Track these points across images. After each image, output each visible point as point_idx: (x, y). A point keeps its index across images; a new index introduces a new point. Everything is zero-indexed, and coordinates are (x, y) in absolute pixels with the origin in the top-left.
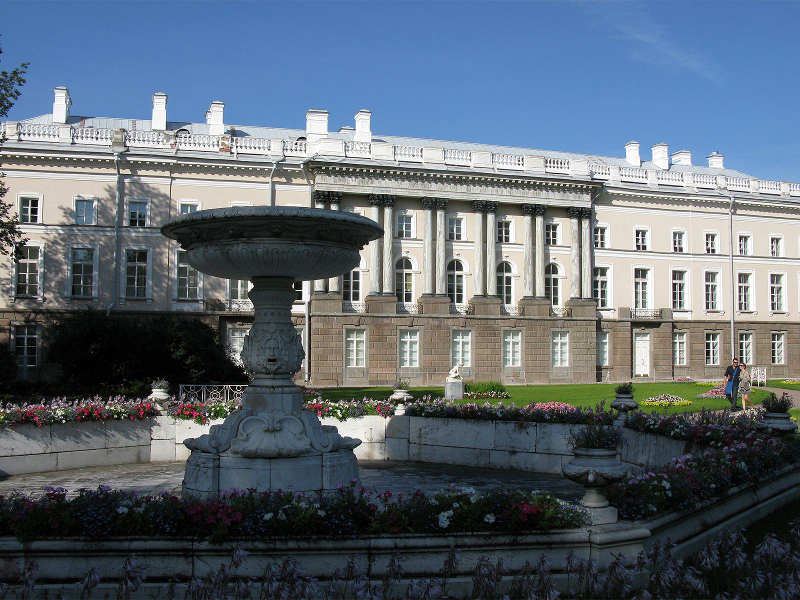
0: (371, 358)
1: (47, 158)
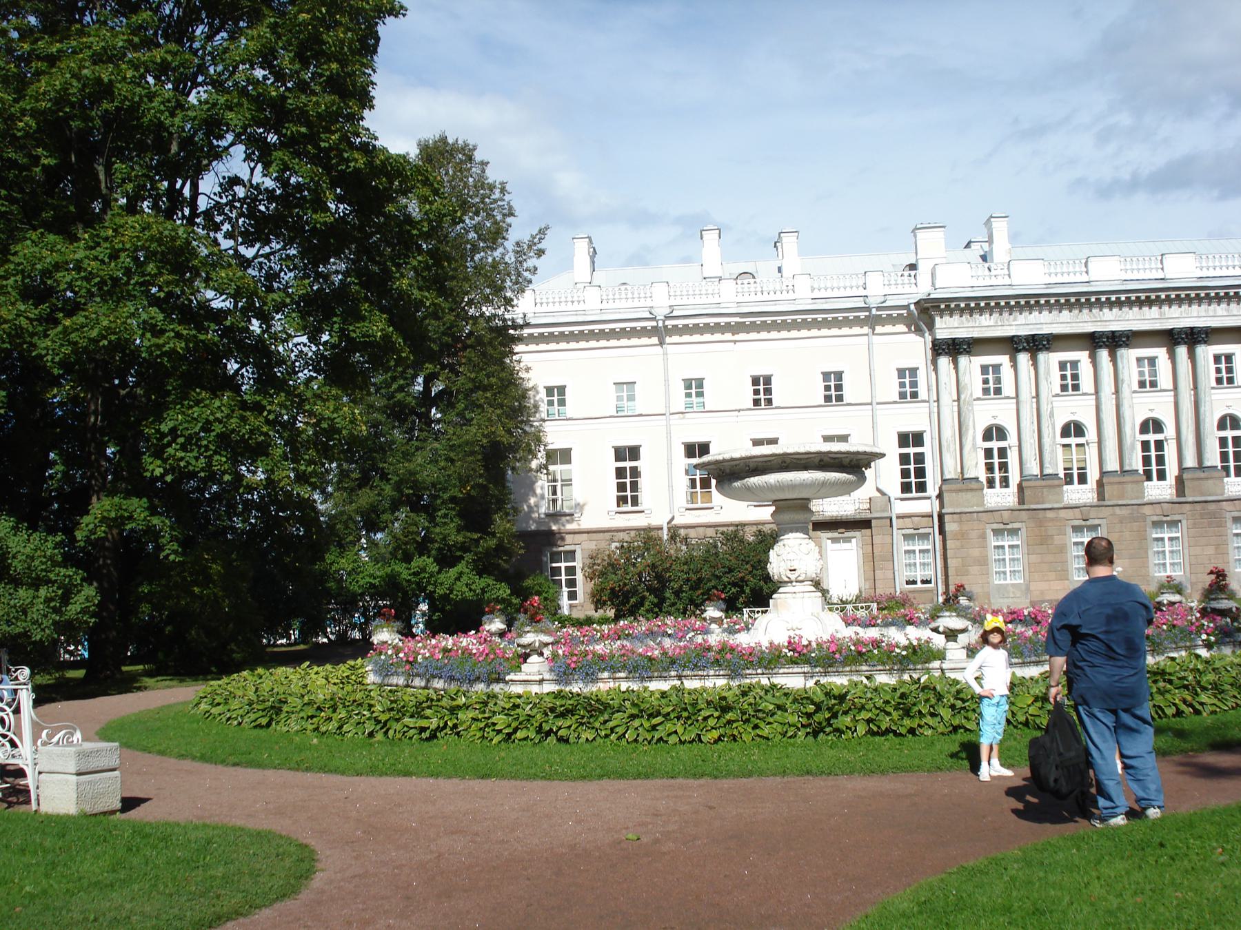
0: (1032, 569)
1: (572, 333)
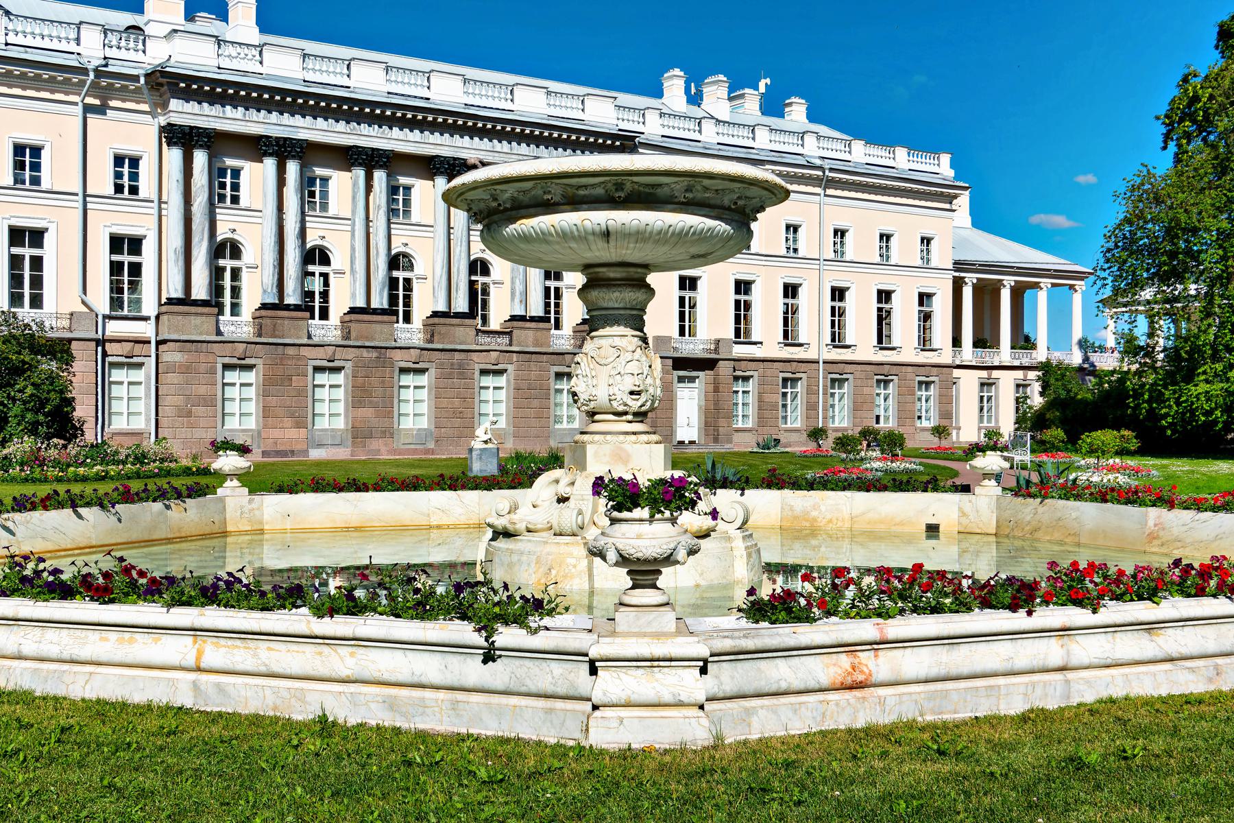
0: (266, 413)
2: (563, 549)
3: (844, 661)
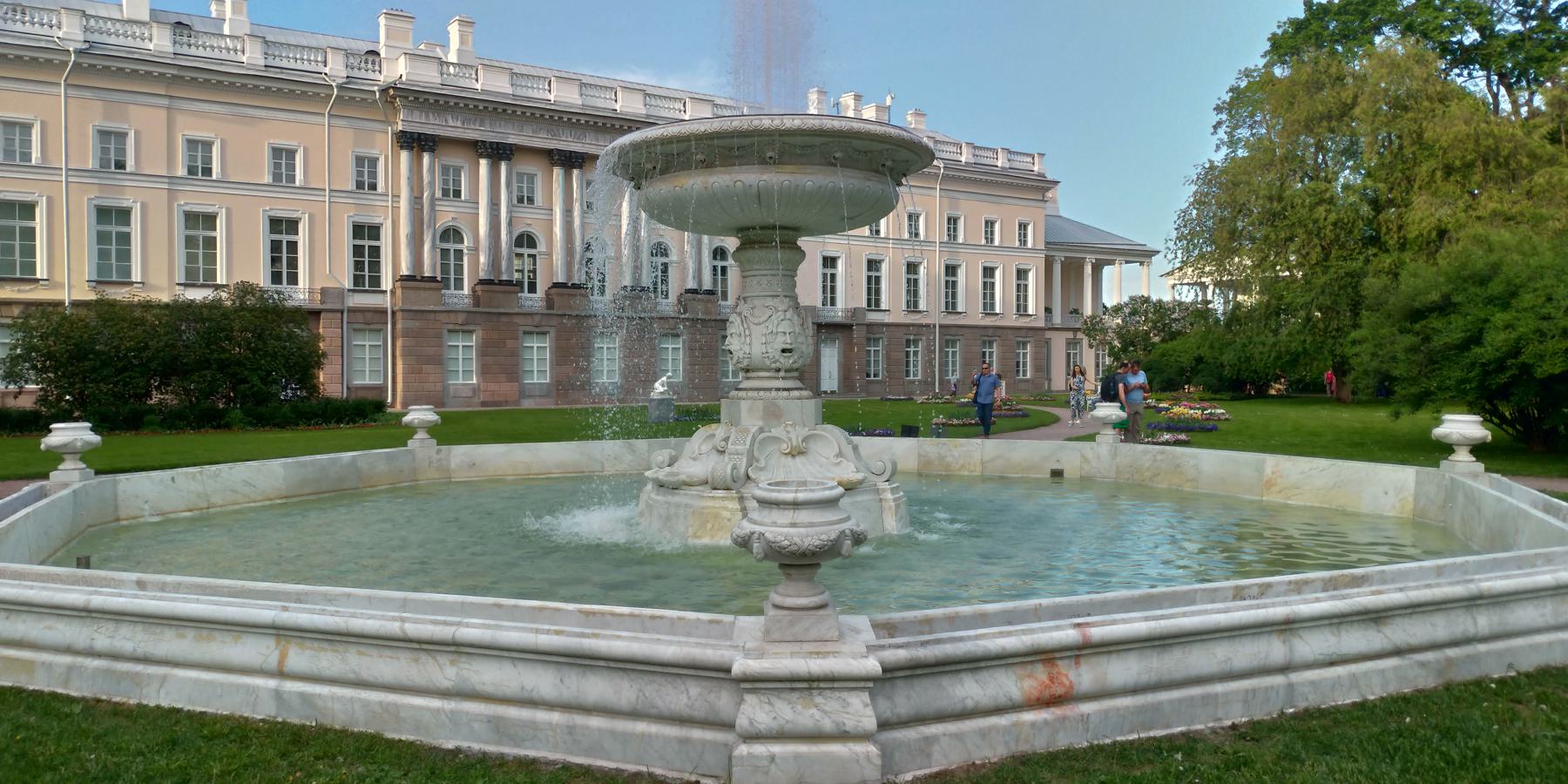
0: (484, 371)
2: (718, 504)
3: (1041, 673)
